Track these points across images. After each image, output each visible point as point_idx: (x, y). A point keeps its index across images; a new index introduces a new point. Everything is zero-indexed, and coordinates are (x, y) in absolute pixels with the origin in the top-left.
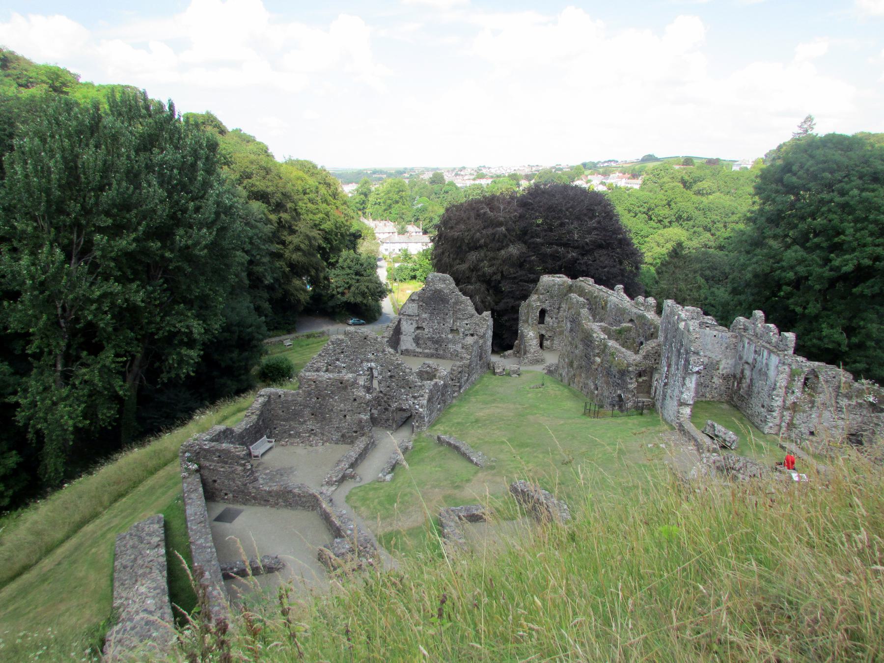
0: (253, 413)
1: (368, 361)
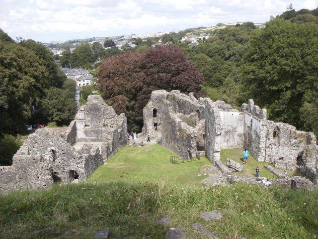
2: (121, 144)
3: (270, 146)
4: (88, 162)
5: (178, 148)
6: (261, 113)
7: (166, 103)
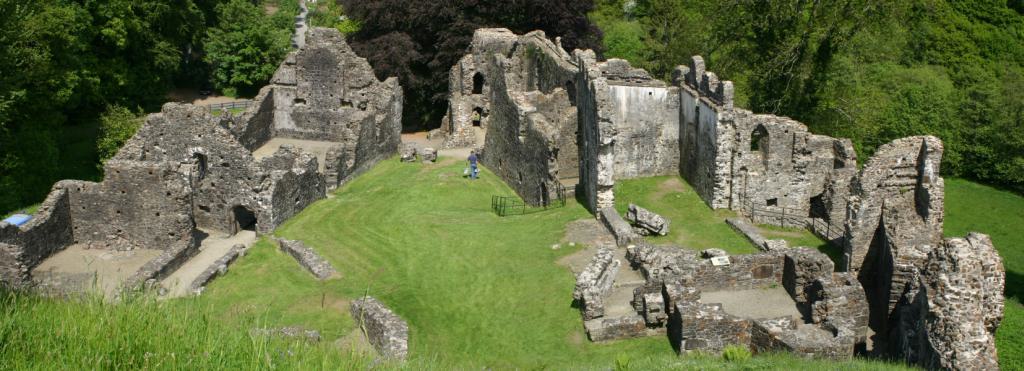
0: (46, 209)
1: (195, 144)
2: (381, 151)
3: (742, 172)
4: (284, 191)
5: (518, 176)
6: (720, 88)
7: (502, 64)
